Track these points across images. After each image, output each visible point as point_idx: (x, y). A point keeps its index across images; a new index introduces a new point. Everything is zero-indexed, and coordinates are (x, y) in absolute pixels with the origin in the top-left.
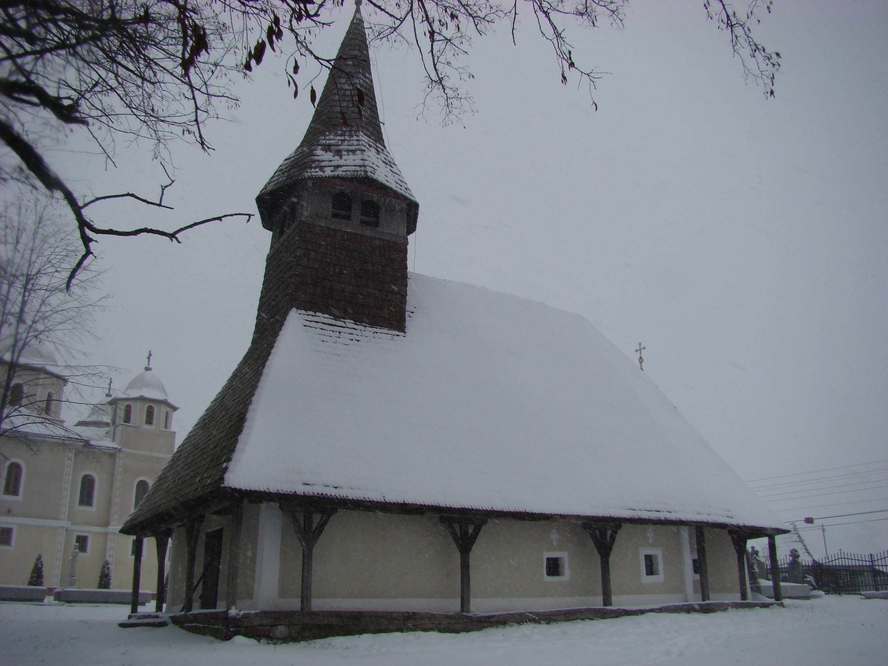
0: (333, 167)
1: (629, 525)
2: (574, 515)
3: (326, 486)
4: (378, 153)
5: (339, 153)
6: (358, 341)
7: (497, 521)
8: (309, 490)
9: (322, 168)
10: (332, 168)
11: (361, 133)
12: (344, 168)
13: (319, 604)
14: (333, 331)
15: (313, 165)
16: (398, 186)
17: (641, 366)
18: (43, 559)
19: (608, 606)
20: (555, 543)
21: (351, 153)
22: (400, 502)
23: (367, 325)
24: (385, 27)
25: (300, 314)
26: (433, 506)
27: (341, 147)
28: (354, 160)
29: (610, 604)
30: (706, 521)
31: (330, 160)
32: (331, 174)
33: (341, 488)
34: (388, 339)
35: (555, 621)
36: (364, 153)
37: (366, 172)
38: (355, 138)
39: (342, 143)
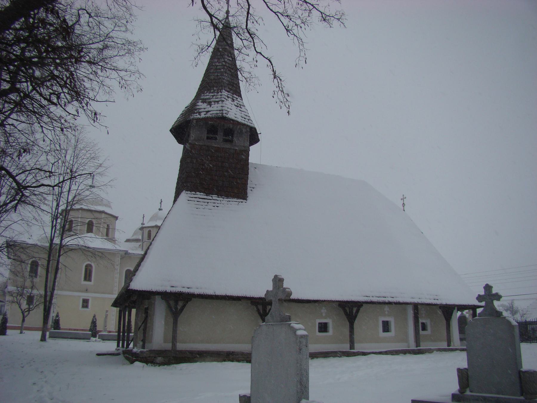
0: (205, 112)
1: (366, 304)
2: (328, 301)
3: (183, 287)
4: (233, 100)
5: (210, 104)
6: (218, 207)
7: (316, 304)
8: (174, 290)
9: (200, 113)
10: (205, 113)
11: (224, 91)
12: (211, 112)
13: (180, 346)
14: (204, 202)
15: (196, 112)
16: (243, 119)
17: (404, 208)
18: (96, 317)
19: (352, 349)
20: (324, 315)
21: (216, 103)
22: (224, 295)
23: (225, 197)
24: (204, 46)
25: (187, 194)
26: (242, 296)
27: (212, 100)
28: (217, 107)
29: (354, 349)
30: (417, 302)
31: (204, 108)
32: (204, 116)
33: (191, 288)
34: (236, 204)
35: (317, 357)
36: (223, 102)
37: (222, 113)
38: (220, 94)
39: (212, 97)
